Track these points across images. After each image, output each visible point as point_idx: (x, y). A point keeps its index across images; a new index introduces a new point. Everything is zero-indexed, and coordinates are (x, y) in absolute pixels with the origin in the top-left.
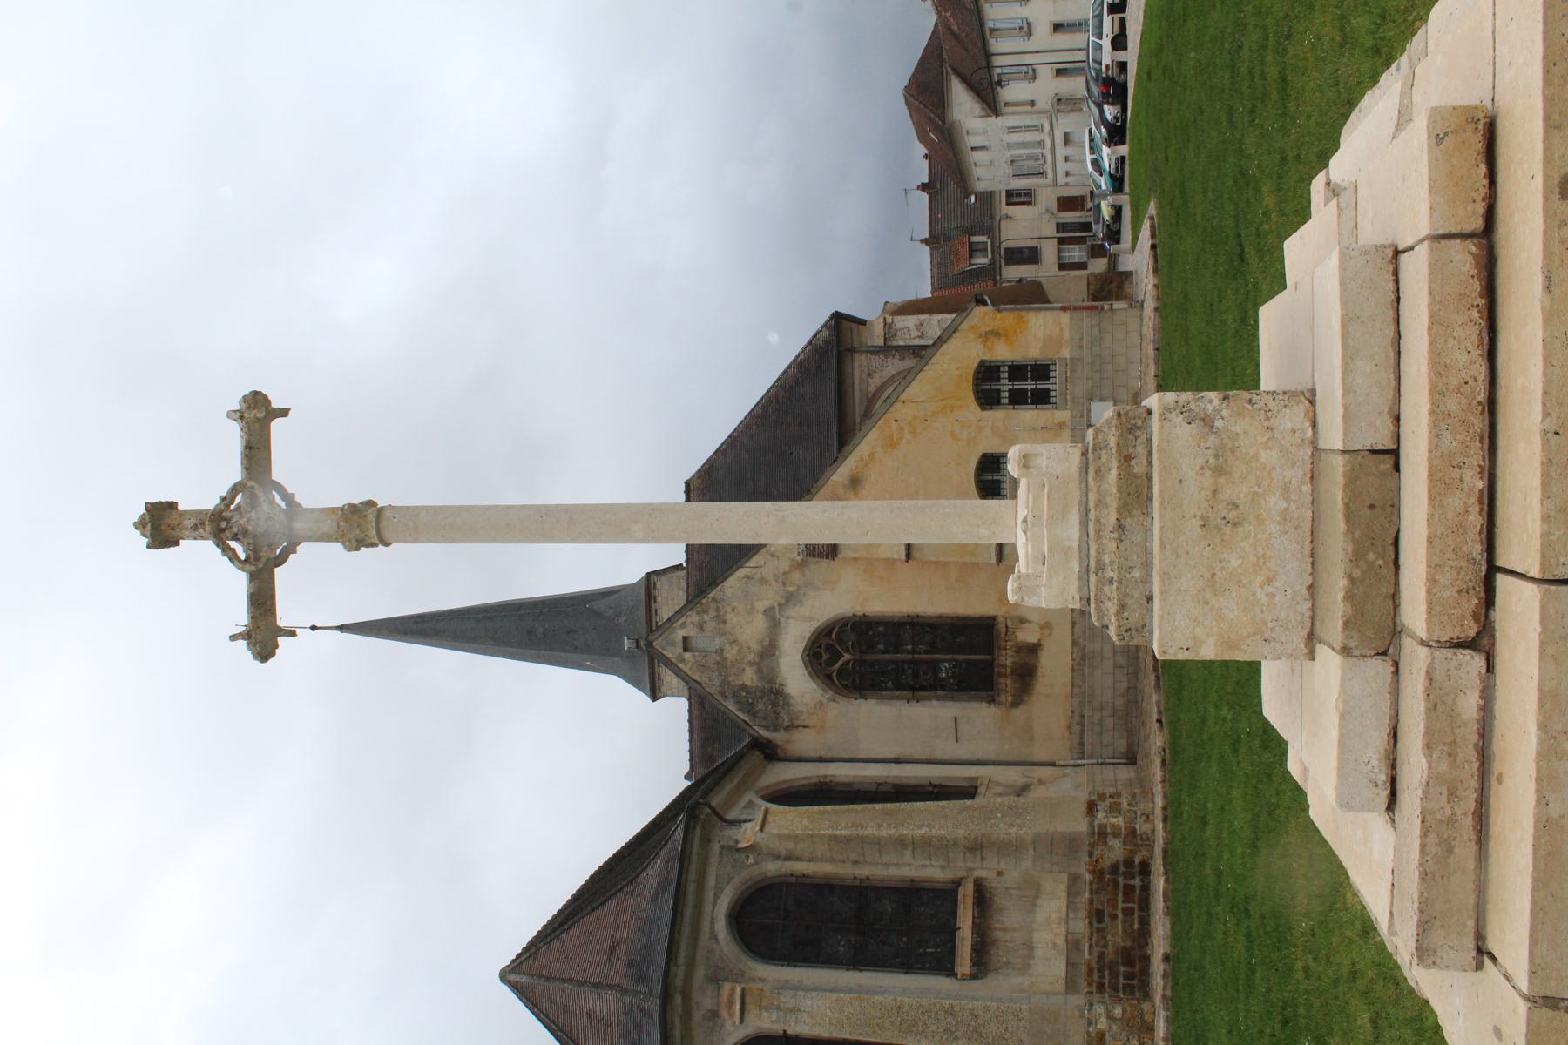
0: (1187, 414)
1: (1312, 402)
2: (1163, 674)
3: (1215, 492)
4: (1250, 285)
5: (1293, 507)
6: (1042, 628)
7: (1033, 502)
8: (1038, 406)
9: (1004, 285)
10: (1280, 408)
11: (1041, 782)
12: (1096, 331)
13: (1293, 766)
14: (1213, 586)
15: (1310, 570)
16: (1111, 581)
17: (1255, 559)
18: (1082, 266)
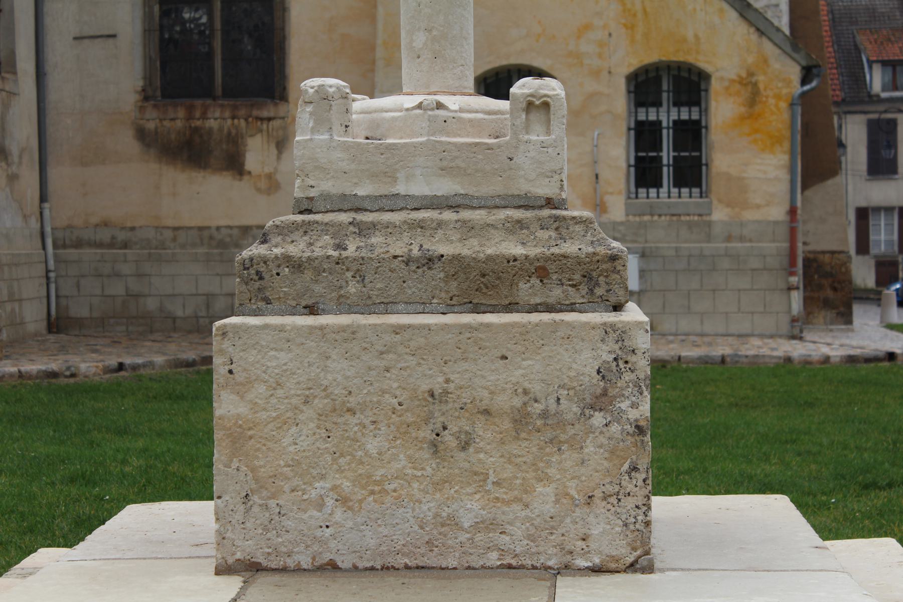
0: (614, 368)
1: (632, 567)
2: (198, 372)
3: (487, 412)
4: (824, 498)
5: (463, 537)
6: (270, 177)
7: (470, 121)
8: (632, 170)
9: (836, 118)
10: (624, 517)
11: (13, 178)
12: (755, 263)
13: (45, 557)
14: (334, 410)
15: (361, 565)
16: (340, 247)
17: (378, 478)
18: (863, 246)
